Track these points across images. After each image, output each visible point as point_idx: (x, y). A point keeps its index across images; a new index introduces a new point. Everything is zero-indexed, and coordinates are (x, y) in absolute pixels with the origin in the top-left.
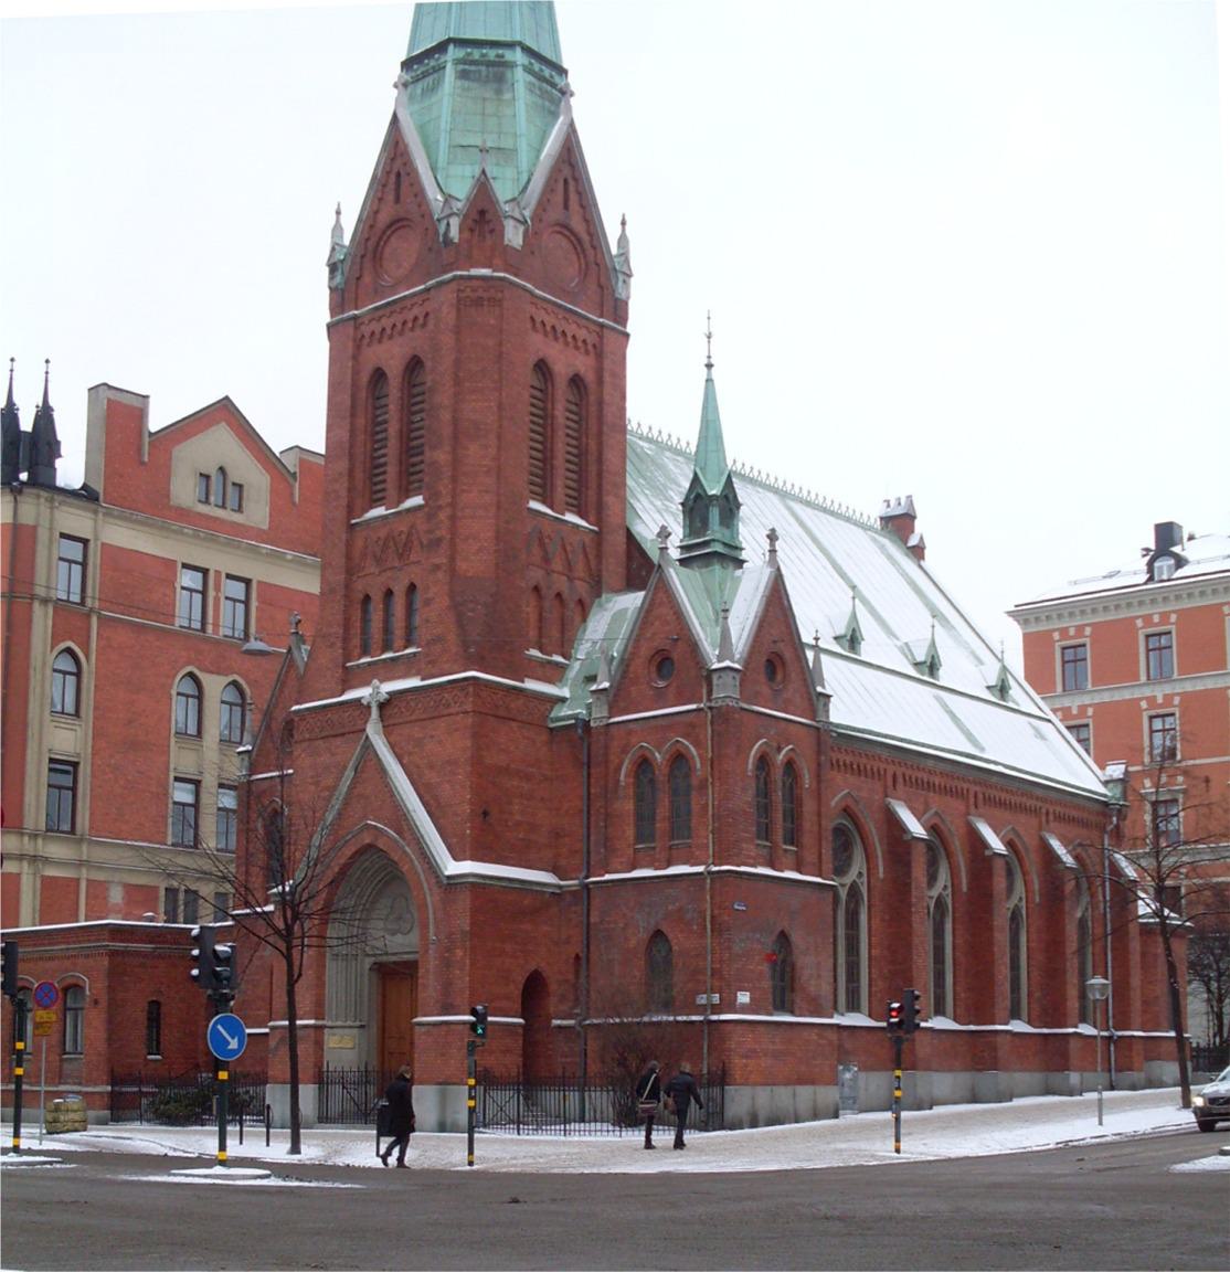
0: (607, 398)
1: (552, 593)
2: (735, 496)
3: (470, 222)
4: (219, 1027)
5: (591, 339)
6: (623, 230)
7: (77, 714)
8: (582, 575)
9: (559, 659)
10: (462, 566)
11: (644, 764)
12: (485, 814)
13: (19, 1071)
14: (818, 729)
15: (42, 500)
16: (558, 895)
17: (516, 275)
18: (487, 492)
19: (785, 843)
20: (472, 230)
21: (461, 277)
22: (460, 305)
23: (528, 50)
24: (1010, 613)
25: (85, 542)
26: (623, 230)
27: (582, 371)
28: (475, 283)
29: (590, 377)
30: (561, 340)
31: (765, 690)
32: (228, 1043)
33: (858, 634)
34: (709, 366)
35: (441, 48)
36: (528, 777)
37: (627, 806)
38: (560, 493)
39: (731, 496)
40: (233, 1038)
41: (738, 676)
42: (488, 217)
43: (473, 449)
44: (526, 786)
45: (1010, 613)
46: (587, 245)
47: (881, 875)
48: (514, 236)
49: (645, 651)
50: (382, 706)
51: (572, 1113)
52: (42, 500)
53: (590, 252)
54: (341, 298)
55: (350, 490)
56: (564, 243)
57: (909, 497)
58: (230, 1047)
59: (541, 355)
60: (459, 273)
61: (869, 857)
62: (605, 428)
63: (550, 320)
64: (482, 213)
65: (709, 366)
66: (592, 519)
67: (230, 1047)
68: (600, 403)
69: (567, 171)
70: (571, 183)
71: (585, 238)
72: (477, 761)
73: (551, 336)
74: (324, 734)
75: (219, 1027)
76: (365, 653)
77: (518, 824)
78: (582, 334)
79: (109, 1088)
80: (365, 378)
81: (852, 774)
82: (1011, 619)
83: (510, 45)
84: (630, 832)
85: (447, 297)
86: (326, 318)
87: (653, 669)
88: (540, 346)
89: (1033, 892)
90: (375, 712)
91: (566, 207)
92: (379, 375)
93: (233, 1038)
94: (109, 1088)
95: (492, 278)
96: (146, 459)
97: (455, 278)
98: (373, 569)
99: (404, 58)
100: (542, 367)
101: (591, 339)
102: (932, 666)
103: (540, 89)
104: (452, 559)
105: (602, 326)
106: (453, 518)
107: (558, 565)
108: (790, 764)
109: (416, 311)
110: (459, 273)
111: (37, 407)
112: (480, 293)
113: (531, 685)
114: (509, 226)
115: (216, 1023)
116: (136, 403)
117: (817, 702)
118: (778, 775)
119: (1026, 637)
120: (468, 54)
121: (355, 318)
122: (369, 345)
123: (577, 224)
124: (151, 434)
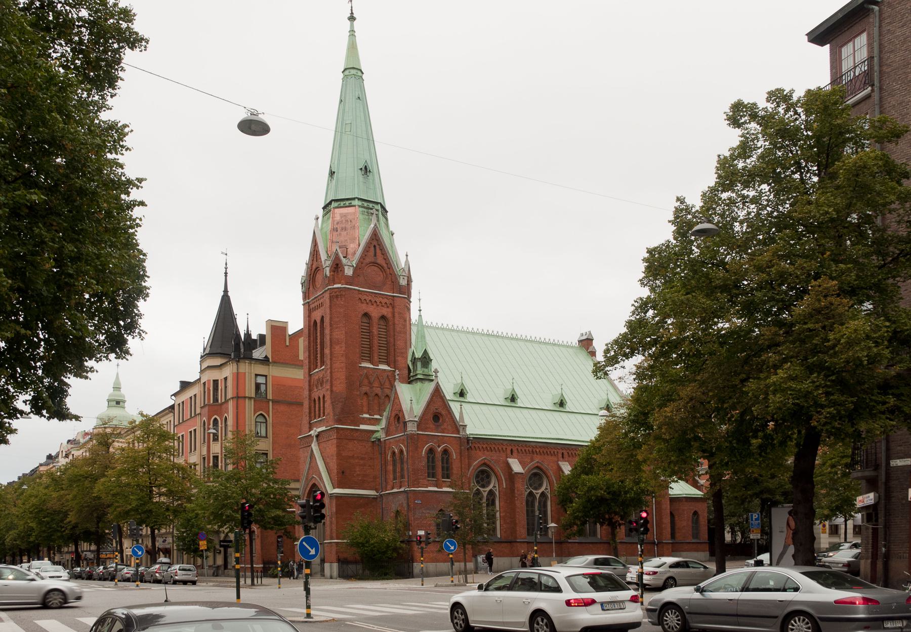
0: (397, 322)
1: (373, 394)
2: (429, 357)
3: (333, 268)
4: (304, 543)
5: (391, 301)
6: (407, 258)
7: (266, 437)
8: (388, 387)
9: (378, 417)
10: (334, 389)
11: (394, 453)
12: (343, 472)
13: (422, 559)
14: (460, 437)
15: (247, 364)
16: (375, 499)
17: (350, 285)
18: (342, 363)
19: (443, 478)
20: (334, 271)
21: (330, 289)
22: (331, 298)
23: (359, 199)
25: (266, 376)
26: (407, 258)
27: (385, 314)
28: (336, 290)
29: (389, 316)
30: (375, 304)
31: (432, 426)
33: (515, 396)
34: (420, 310)
35: (330, 203)
36: (362, 459)
38: (376, 358)
39: (427, 357)
41: (416, 423)
42: (339, 266)
43: (337, 348)
44: (362, 462)
46: (386, 268)
48: (349, 272)
49: (393, 415)
50: (317, 436)
52: (247, 364)
53: (388, 270)
56: (376, 268)
57: (590, 332)
59: (365, 311)
60: (329, 287)
61: (499, 480)
62: (396, 334)
64: (337, 265)
65: (420, 310)
66: (393, 367)
68: (394, 324)
69: (375, 243)
70: (377, 247)
71: (385, 265)
72: (339, 455)
73: (370, 304)
75: (304, 543)
76: (315, 418)
77: (358, 475)
79: (262, 566)
80: (312, 323)
81: (488, 451)
83: (354, 199)
84: (391, 476)
85: (327, 295)
87: (396, 423)
88: (364, 308)
91: (375, 255)
94: (262, 566)
95: (341, 288)
96: (288, 344)
97: (328, 289)
98: (316, 390)
99: (323, 206)
100: (366, 315)
101: (391, 301)
102: (562, 404)
103: (367, 212)
104: (331, 386)
105: (394, 296)
106: (331, 372)
107: (376, 384)
108: (446, 452)
110: (329, 287)
112: (337, 293)
113: (362, 427)
114: (346, 268)
116: (281, 325)
117: (457, 427)
118: (438, 456)
120: (345, 204)
121: (308, 302)
123: (380, 260)
124: (289, 335)
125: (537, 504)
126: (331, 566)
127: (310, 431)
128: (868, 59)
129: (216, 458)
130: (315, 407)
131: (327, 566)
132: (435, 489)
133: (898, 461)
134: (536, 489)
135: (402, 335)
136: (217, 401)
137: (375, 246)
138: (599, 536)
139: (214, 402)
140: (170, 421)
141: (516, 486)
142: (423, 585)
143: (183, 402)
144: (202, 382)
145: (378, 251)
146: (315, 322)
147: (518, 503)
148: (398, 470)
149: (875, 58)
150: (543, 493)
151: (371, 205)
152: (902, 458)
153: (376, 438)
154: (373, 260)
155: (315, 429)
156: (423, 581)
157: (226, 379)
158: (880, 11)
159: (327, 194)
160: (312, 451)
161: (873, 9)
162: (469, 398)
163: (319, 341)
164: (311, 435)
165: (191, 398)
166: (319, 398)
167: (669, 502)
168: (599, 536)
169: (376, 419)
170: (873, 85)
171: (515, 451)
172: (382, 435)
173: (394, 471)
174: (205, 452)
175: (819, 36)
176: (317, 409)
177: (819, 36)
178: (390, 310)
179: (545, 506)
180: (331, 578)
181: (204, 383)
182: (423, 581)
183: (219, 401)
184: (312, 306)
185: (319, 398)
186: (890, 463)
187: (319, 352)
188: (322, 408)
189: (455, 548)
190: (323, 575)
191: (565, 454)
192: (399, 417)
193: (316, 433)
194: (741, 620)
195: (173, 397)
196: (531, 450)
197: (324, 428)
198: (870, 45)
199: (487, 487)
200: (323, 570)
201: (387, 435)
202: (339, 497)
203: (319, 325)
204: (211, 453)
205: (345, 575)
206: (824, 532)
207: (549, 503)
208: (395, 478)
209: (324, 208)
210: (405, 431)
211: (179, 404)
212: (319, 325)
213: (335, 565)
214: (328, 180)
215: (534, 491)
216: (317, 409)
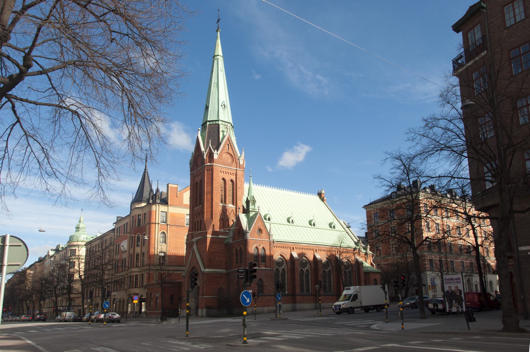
4: (244, 295)
11: (237, 250)
12: (210, 260)
24: (363, 207)
31: (256, 235)
32: (247, 300)
37: (235, 257)
40: (248, 299)
45: (363, 207)
47: (290, 266)
50: (196, 242)
51: (97, 290)
53: (234, 157)
54: (192, 170)
55: (193, 204)
58: (247, 302)
63: (225, 171)
67: (247, 302)
69: (228, 143)
70: (229, 145)
71: (233, 154)
74: (461, 180)
75: (244, 295)
78: (232, 172)
80: (195, 184)
82: (363, 208)
86: (190, 173)
89: (387, 263)
90: (195, 243)
92: (197, 183)
93: (248, 299)
100: (224, 179)
109: (201, 171)
111: (192, 154)
115: (243, 294)
119: (367, 212)
121: (193, 173)
122: (99, 244)
125: (280, 275)
126: (202, 311)
127: (192, 239)
128: (482, 38)
129: (138, 255)
130: (195, 227)
131: (200, 311)
132: (264, 268)
133: (523, 247)
134: (304, 268)
135: (241, 190)
136: (140, 226)
137: (228, 145)
138: (310, 292)
139: (138, 226)
140: (112, 237)
141: (295, 266)
142: (255, 319)
143: (120, 227)
144: (132, 215)
145: (230, 147)
146: (197, 183)
147: (296, 275)
148: (124, 264)
149: (487, 36)
150: (307, 270)
151: (226, 124)
152: (524, 246)
153: (227, 242)
154: (227, 152)
155: (195, 238)
156: (255, 317)
157: (145, 214)
158: (486, 12)
159: (204, 118)
160: (194, 249)
161: (483, 11)
162: (272, 221)
163: (198, 193)
164: (193, 241)
165: (124, 225)
166: (198, 222)
167: (363, 274)
168: (310, 292)
169: (227, 232)
170: (487, 50)
171: (295, 248)
172: (231, 241)
173: (237, 259)
174: (132, 252)
175: (457, 28)
176: (196, 227)
177: (457, 28)
178: (235, 176)
179: (284, 276)
180: (202, 316)
181: (133, 217)
182: (255, 317)
183: (141, 226)
184: (195, 175)
185: (198, 222)
186: (518, 249)
187: (198, 198)
188: (199, 227)
189: (250, 300)
190: (197, 315)
191: (317, 250)
192: (240, 231)
193: (196, 240)
194: (74, 325)
195: (114, 225)
196: (290, 246)
197: (200, 238)
198: (482, 30)
199: (282, 267)
200: (197, 312)
201: (233, 240)
202: (208, 274)
203: (199, 184)
204: (135, 252)
205: (209, 316)
206: (430, 290)
207: (310, 275)
208: (237, 263)
209: (202, 125)
210: (244, 238)
211: (117, 228)
212: (199, 184)
213: (205, 310)
214: (205, 111)
215: (303, 269)
216: (196, 227)
